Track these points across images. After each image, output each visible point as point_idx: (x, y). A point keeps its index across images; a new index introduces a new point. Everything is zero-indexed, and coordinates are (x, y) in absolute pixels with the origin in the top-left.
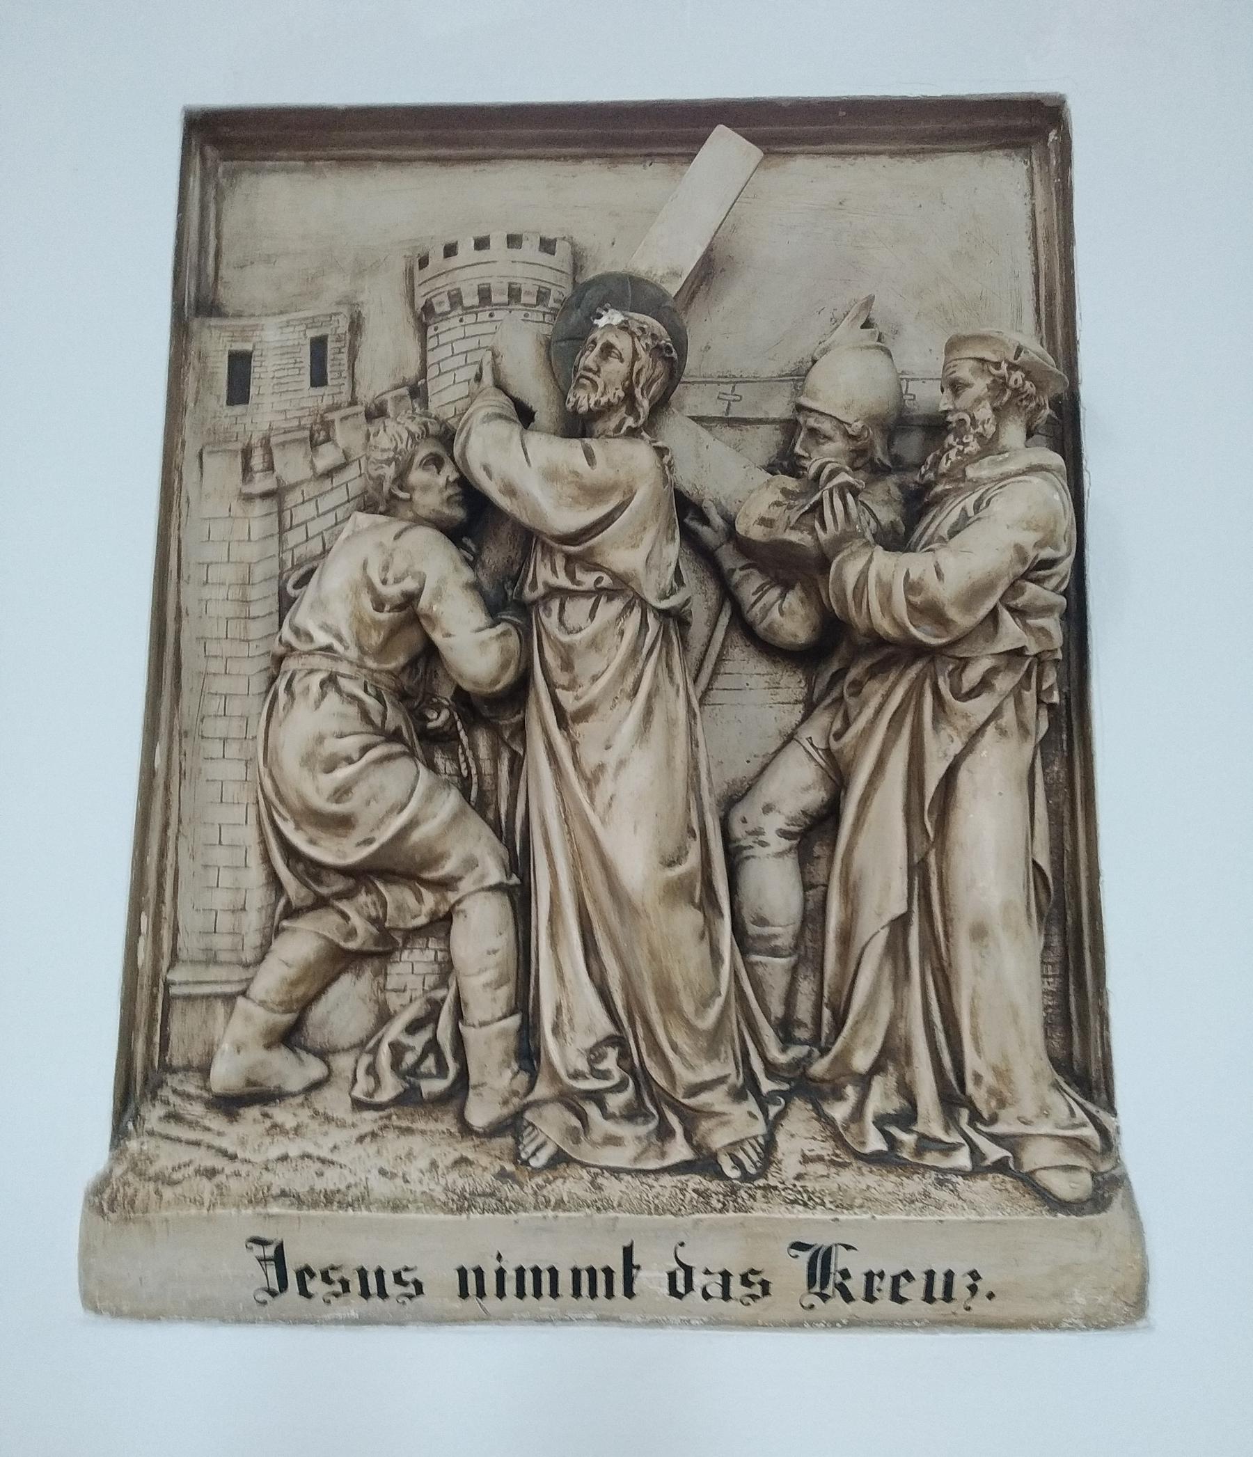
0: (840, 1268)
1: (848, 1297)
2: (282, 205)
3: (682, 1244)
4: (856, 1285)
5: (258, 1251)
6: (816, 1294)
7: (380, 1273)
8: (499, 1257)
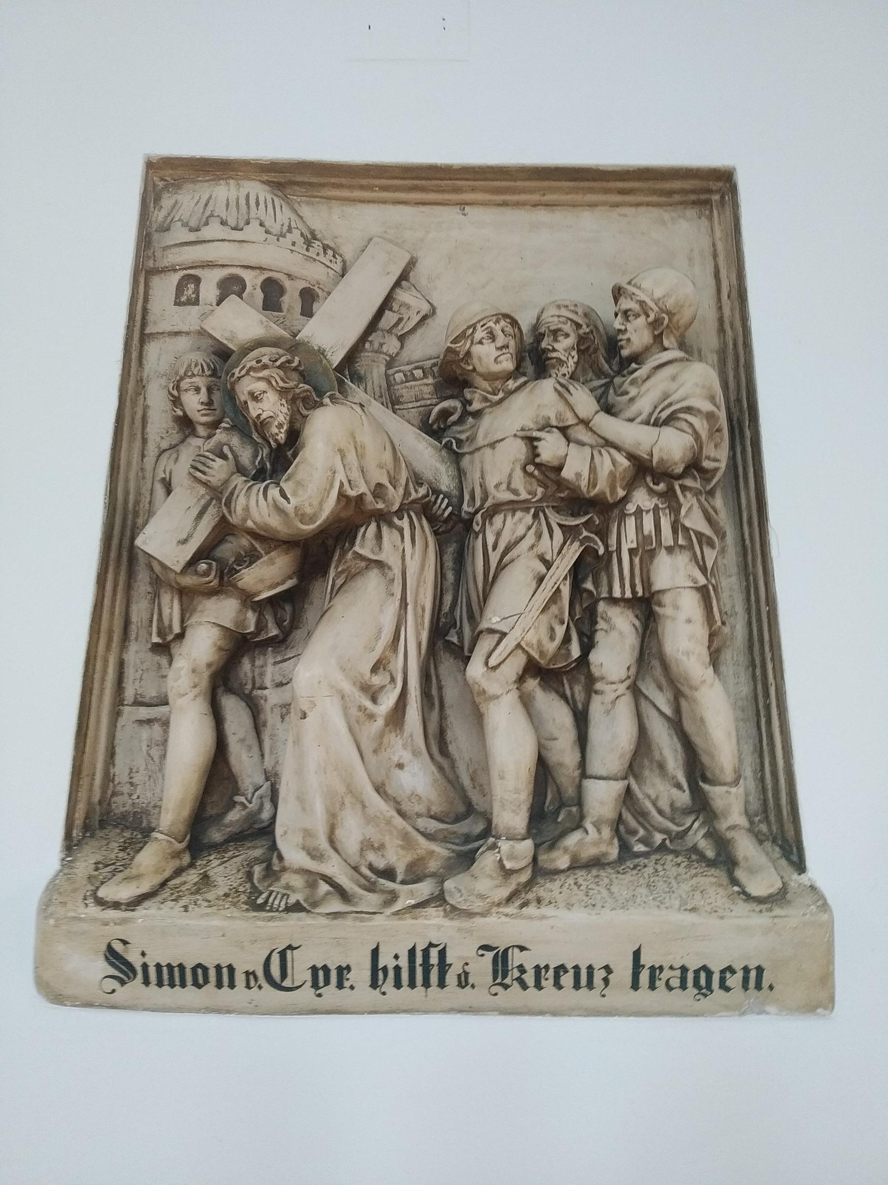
0: (516, 964)
1: (524, 986)
2: (187, 201)
6: (499, 984)
7: (590, 968)
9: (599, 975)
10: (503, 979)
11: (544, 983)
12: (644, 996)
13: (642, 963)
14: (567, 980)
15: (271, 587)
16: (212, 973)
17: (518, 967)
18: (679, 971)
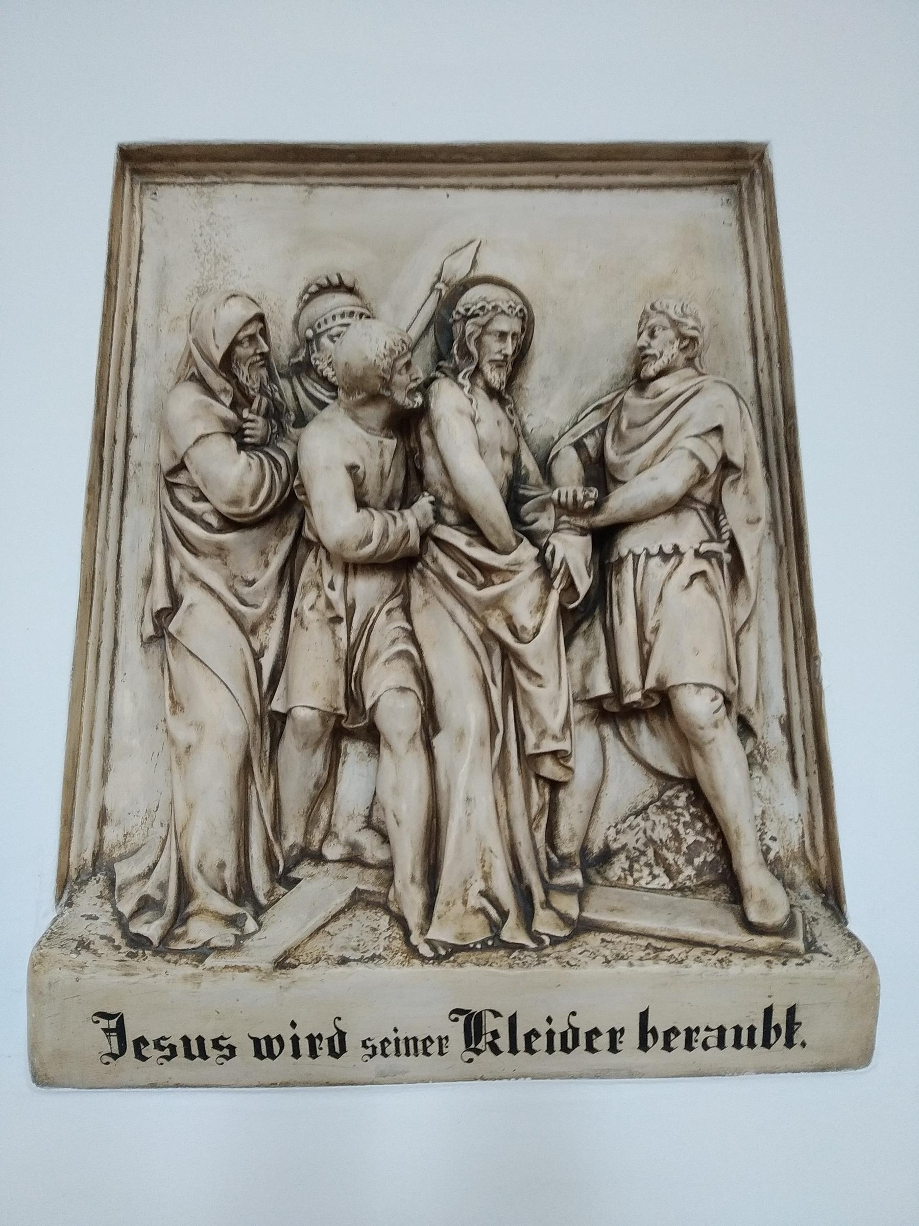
1: (496, 1051)
2: (174, 205)
3: (574, 1014)
5: (104, 1023)
7: (200, 1040)
8: (549, 1020)
10: (476, 1045)
11: (319, 1052)
13: (796, 1020)
14: (678, 1042)
15: (618, 593)
18: (716, 1031)
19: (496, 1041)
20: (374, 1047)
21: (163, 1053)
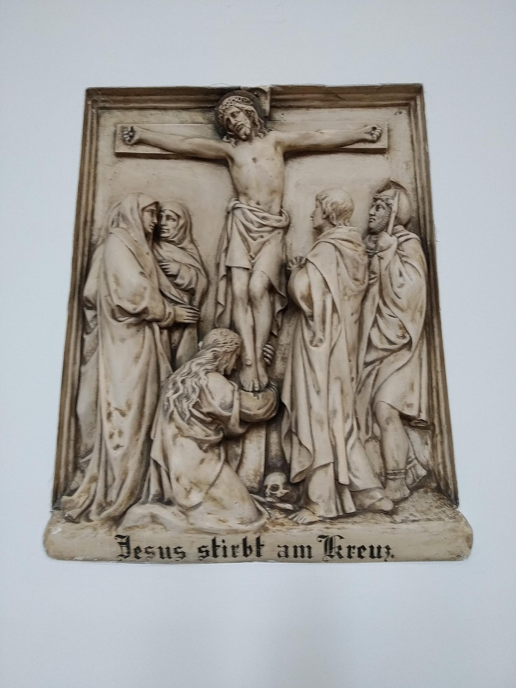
0: (337, 545)
1: (341, 557)
4: (344, 552)
5: (119, 540)
7: (168, 548)
9: (383, 551)
12: (146, 561)
13: (217, 544)
14: (366, 553)
16: (229, 552)
17: (166, 548)
19: (340, 551)
20: (176, 552)
21: (201, 554)
